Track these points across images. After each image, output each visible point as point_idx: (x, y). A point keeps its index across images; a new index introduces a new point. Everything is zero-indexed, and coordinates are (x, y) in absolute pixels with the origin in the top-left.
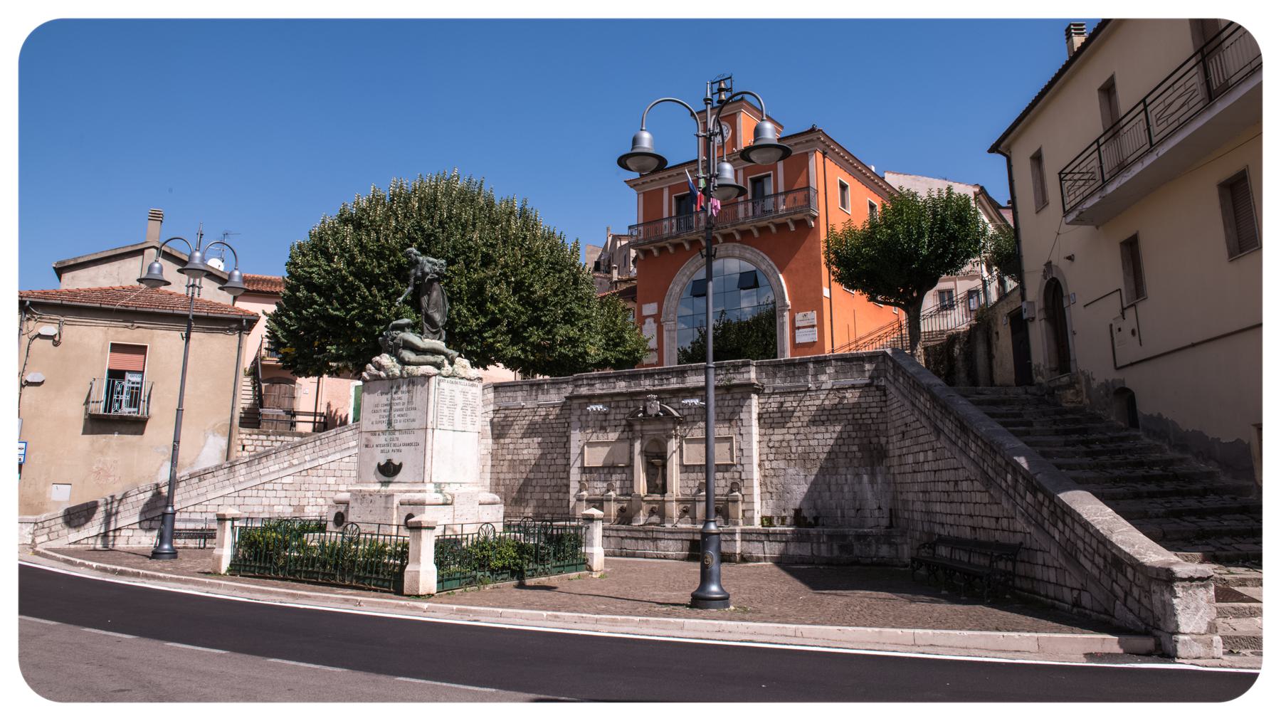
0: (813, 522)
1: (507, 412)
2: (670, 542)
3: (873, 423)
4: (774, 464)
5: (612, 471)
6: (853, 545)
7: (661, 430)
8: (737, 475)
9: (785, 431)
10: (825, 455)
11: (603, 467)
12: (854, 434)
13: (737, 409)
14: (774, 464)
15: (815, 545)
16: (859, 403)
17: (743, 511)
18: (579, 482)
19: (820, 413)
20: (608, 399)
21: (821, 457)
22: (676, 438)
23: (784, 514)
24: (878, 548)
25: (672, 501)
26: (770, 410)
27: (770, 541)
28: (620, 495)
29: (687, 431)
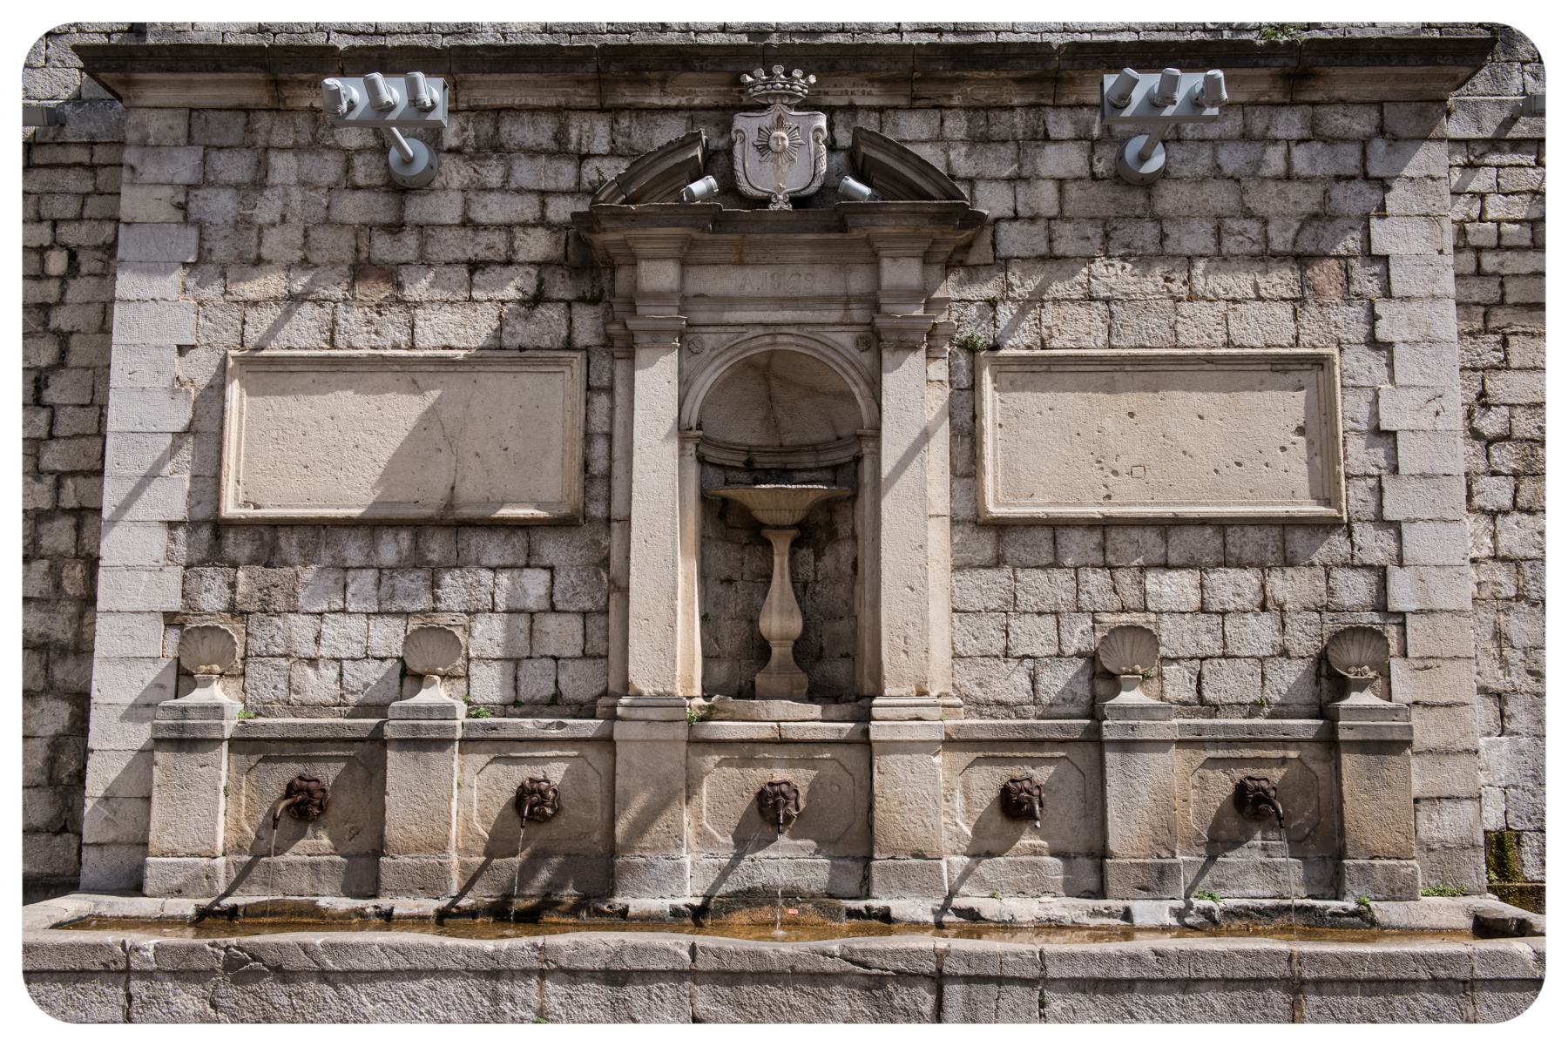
5: (436, 548)
7: (826, 300)
8: (1355, 589)
11: (371, 526)
18: (171, 619)
28: (504, 709)
29: (1005, 313)
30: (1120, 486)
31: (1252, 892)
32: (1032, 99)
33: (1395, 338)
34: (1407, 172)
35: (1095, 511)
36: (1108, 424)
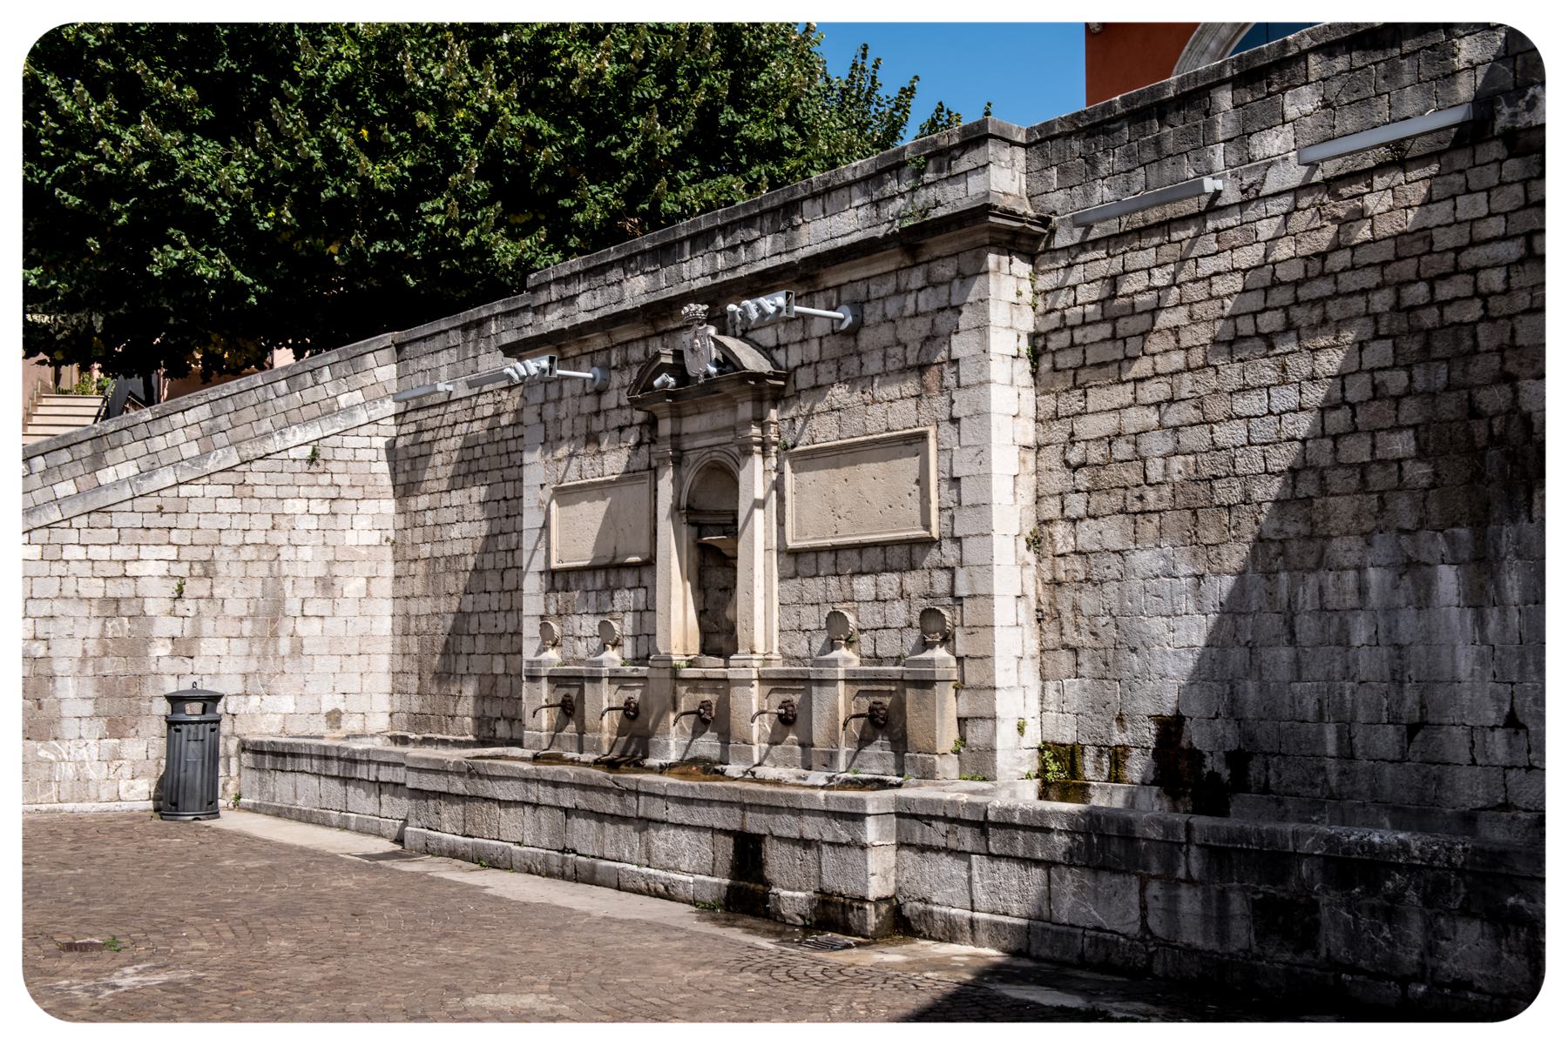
0: (1226, 774)
1: (421, 415)
2: (684, 837)
3: (1486, 318)
4: (1087, 535)
6: (1314, 907)
8: (941, 581)
9: (1123, 394)
10: (1275, 486)
11: (592, 569)
12: (1397, 381)
13: (943, 322)
14: (1087, 535)
15: (1154, 889)
16: (1423, 233)
17: (962, 721)
18: (542, 617)
19: (1255, 301)
20: (599, 341)
21: (1258, 493)
22: (765, 454)
23: (1118, 738)
24: (1433, 934)
25: (747, 682)
26: (1074, 314)
27: (992, 856)
29: (799, 423)
30: (843, 524)
31: (874, 771)
32: (805, 291)
33: (961, 415)
34: (970, 299)
35: (828, 542)
36: (837, 487)
